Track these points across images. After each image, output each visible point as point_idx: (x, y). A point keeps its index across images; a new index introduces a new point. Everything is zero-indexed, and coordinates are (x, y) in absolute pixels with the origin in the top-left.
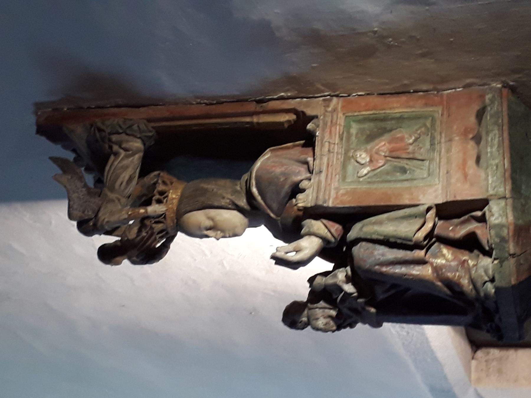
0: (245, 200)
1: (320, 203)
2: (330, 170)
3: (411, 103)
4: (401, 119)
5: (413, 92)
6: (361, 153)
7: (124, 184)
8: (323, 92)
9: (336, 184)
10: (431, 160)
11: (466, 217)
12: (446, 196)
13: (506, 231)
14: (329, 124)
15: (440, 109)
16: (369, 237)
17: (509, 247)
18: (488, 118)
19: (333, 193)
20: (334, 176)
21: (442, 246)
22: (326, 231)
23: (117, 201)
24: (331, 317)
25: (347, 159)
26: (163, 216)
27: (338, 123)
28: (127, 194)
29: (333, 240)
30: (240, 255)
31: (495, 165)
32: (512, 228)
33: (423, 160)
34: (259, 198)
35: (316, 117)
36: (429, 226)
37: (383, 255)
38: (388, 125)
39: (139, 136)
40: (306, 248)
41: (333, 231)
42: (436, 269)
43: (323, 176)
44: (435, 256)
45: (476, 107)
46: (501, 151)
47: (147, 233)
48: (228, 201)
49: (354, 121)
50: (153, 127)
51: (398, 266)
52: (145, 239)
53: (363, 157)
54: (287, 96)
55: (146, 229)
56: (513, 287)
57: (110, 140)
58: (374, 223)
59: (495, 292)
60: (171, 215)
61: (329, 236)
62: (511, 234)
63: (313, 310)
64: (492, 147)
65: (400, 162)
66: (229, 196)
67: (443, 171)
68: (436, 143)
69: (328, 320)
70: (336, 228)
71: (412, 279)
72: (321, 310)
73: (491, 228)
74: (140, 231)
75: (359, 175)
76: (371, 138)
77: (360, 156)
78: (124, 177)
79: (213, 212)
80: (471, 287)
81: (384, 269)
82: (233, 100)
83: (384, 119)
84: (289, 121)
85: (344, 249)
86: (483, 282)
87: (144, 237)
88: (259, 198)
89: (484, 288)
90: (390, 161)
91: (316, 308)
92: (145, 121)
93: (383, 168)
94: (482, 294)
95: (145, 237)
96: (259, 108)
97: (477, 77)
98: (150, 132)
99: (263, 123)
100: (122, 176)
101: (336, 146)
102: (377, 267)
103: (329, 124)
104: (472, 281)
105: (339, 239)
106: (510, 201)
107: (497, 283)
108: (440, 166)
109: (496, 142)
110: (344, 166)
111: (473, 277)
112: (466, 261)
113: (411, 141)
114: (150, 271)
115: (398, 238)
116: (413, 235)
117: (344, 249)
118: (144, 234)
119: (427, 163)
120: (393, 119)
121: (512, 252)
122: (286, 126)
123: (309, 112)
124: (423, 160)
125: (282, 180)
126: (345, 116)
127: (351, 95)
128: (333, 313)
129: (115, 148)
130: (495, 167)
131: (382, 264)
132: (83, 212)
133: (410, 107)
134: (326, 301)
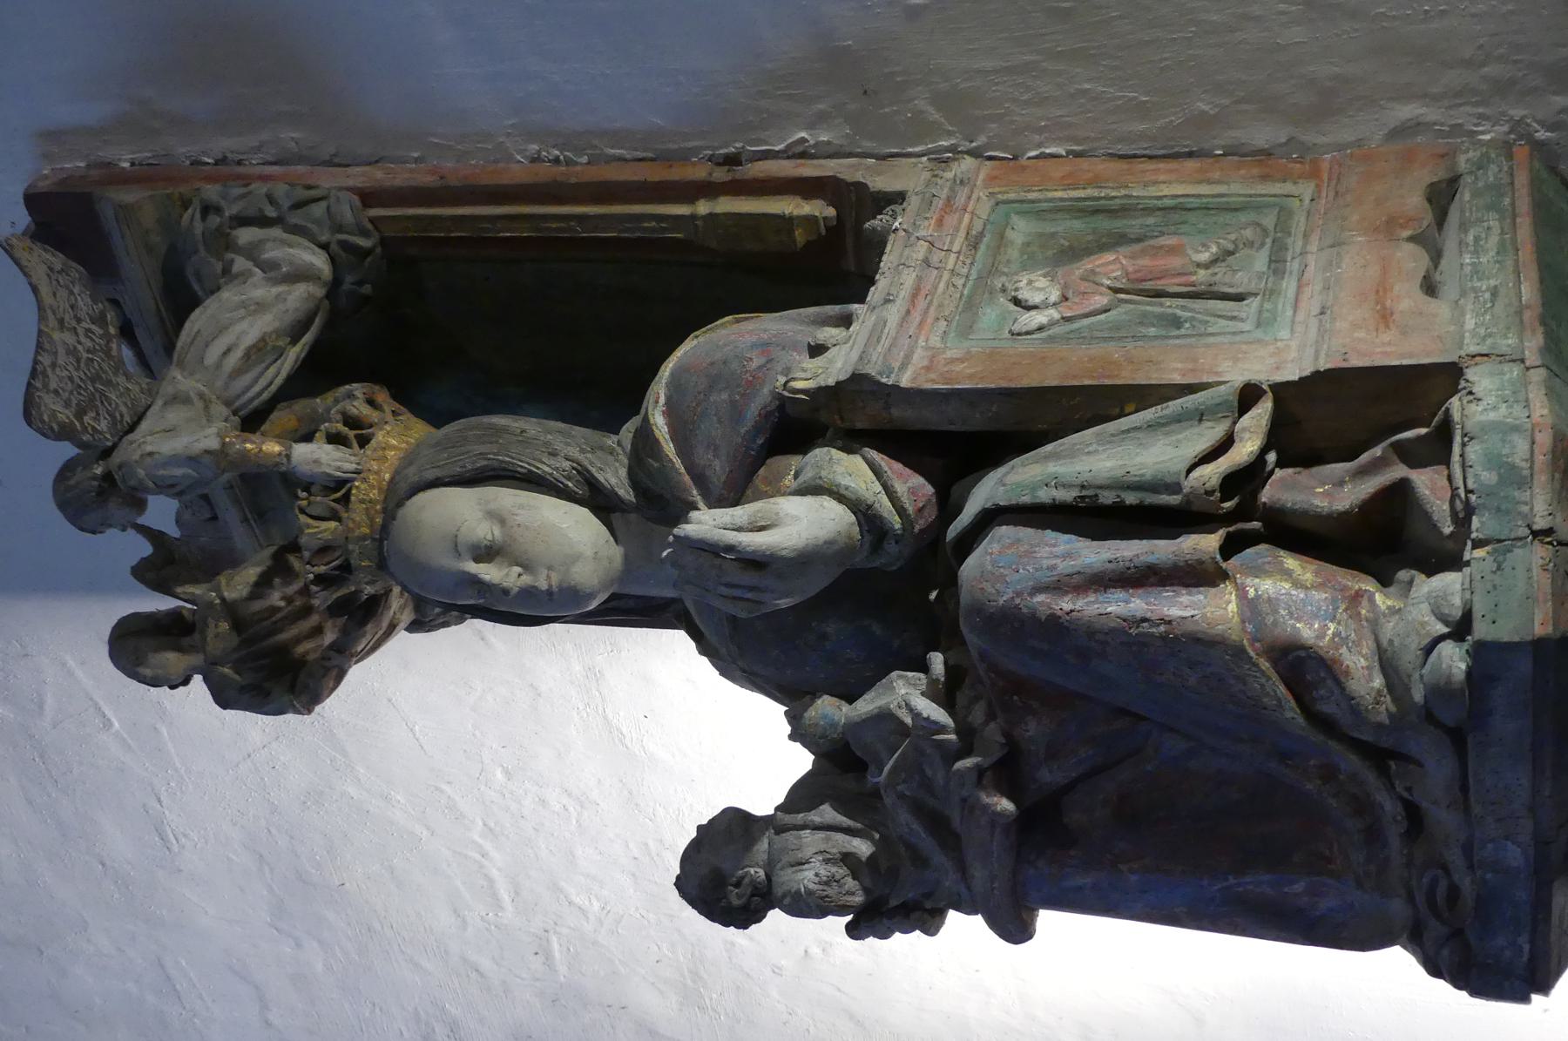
0: (623, 472)
1: (871, 370)
2: (921, 304)
3: (1217, 175)
4: (1177, 210)
5: (1223, 155)
6: (1033, 277)
7: (238, 354)
8: (935, 131)
9: (935, 341)
10: (1271, 293)
11: (1377, 451)
12: (1316, 358)
13: (1521, 446)
14: (939, 204)
15: (1306, 189)
16: (1026, 499)
17: (1530, 503)
18: (1467, 197)
19: (920, 359)
20: (929, 320)
21: (1282, 553)
22: (878, 487)
23: (199, 404)
24: (847, 859)
25: (982, 289)
26: (339, 487)
27: (970, 208)
28: (239, 396)
29: (896, 522)
30: (605, 912)
31: (1487, 290)
32: (1544, 439)
33: (1239, 298)
34: (669, 449)
35: (899, 197)
36: (1245, 449)
37: (1067, 556)
38: (1134, 225)
39: (324, 238)
40: (796, 518)
41: (900, 488)
42: (1251, 607)
43: (893, 314)
44: (1258, 572)
45: (1426, 174)
46: (1509, 263)
47: (289, 600)
48: (567, 465)
49: (1018, 213)
50: (372, 220)
51: (1119, 594)
52: (279, 616)
53: (1039, 287)
54: (817, 144)
55: (287, 583)
56: (1539, 644)
57: (230, 246)
58: (1047, 458)
59: (1469, 673)
60: (367, 492)
61: (885, 506)
62: (1540, 459)
63: (790, 837)
64: (1476, 253)
65: (1161, 305)
66: (574, 452)
67: (1311, 305)
68: (1289, 259)
69: (840, 871)
70: (912, 486)
71: (1163, 637)
72: (821, 835)
73: (1472, 439)
74: (263, 584)
75: (1016, 328)
76: (1072, 253)
77: (1030, 282)
78: (244, 332)
79: (506, 498)
80: (1378, 682)
81: (1065, 604)
82: (644, 155)
83: (1124, 211)
84: (810, 220)
85: (933, 596)
86: (1426, 641)
87: (274, 610)
88: (669, 449)
89: (1428, 666)
90: (1126, 301)
91: (804, 827)
92: (356, 199)
93: (1102, 317)
94: (1418, 695)
95: (279, 609)
96: (721, 175)
97: (1436, 98)
98: (364, 233)
99: (725, 214)
100: (238, 328)
101: (953, 257)
102: (1040, 598)
103: (939, 204)
104: (1386, 662)
105: (917, 528)
106: (1538, 375)
107: (1482, 630)
108: (1294, 303)
109: (1494, 240)
110: (970, 306)
111: (1385, 643)
112: (1366, 597)
113: (1204, 257)
114: (319, 967)
115: (1128, 487)
116: (1186, 465)
117: (933, 596)
118: (275, 598)
119: (1253, 304)
120: (1149, 211)
121: (1540, 523)
122: (800, 236)
123: (881, 182)
124: (1239, 298)
125: (754, 364)
126: (993, 202)
127: (1024, 154)
128: (863, 848)
129: (240, 264)
130: (1487, 295)
131: (1059, 586)
132: (80, 414)
133: (1209, 182)
134: (841, 806)
